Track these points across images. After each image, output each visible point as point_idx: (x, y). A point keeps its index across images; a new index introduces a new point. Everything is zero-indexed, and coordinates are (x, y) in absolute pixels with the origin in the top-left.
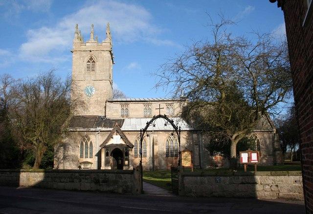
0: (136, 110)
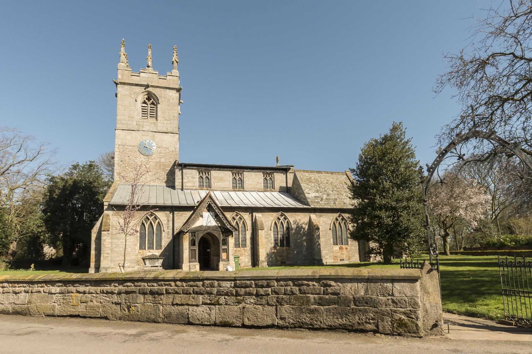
0: (221, 179)
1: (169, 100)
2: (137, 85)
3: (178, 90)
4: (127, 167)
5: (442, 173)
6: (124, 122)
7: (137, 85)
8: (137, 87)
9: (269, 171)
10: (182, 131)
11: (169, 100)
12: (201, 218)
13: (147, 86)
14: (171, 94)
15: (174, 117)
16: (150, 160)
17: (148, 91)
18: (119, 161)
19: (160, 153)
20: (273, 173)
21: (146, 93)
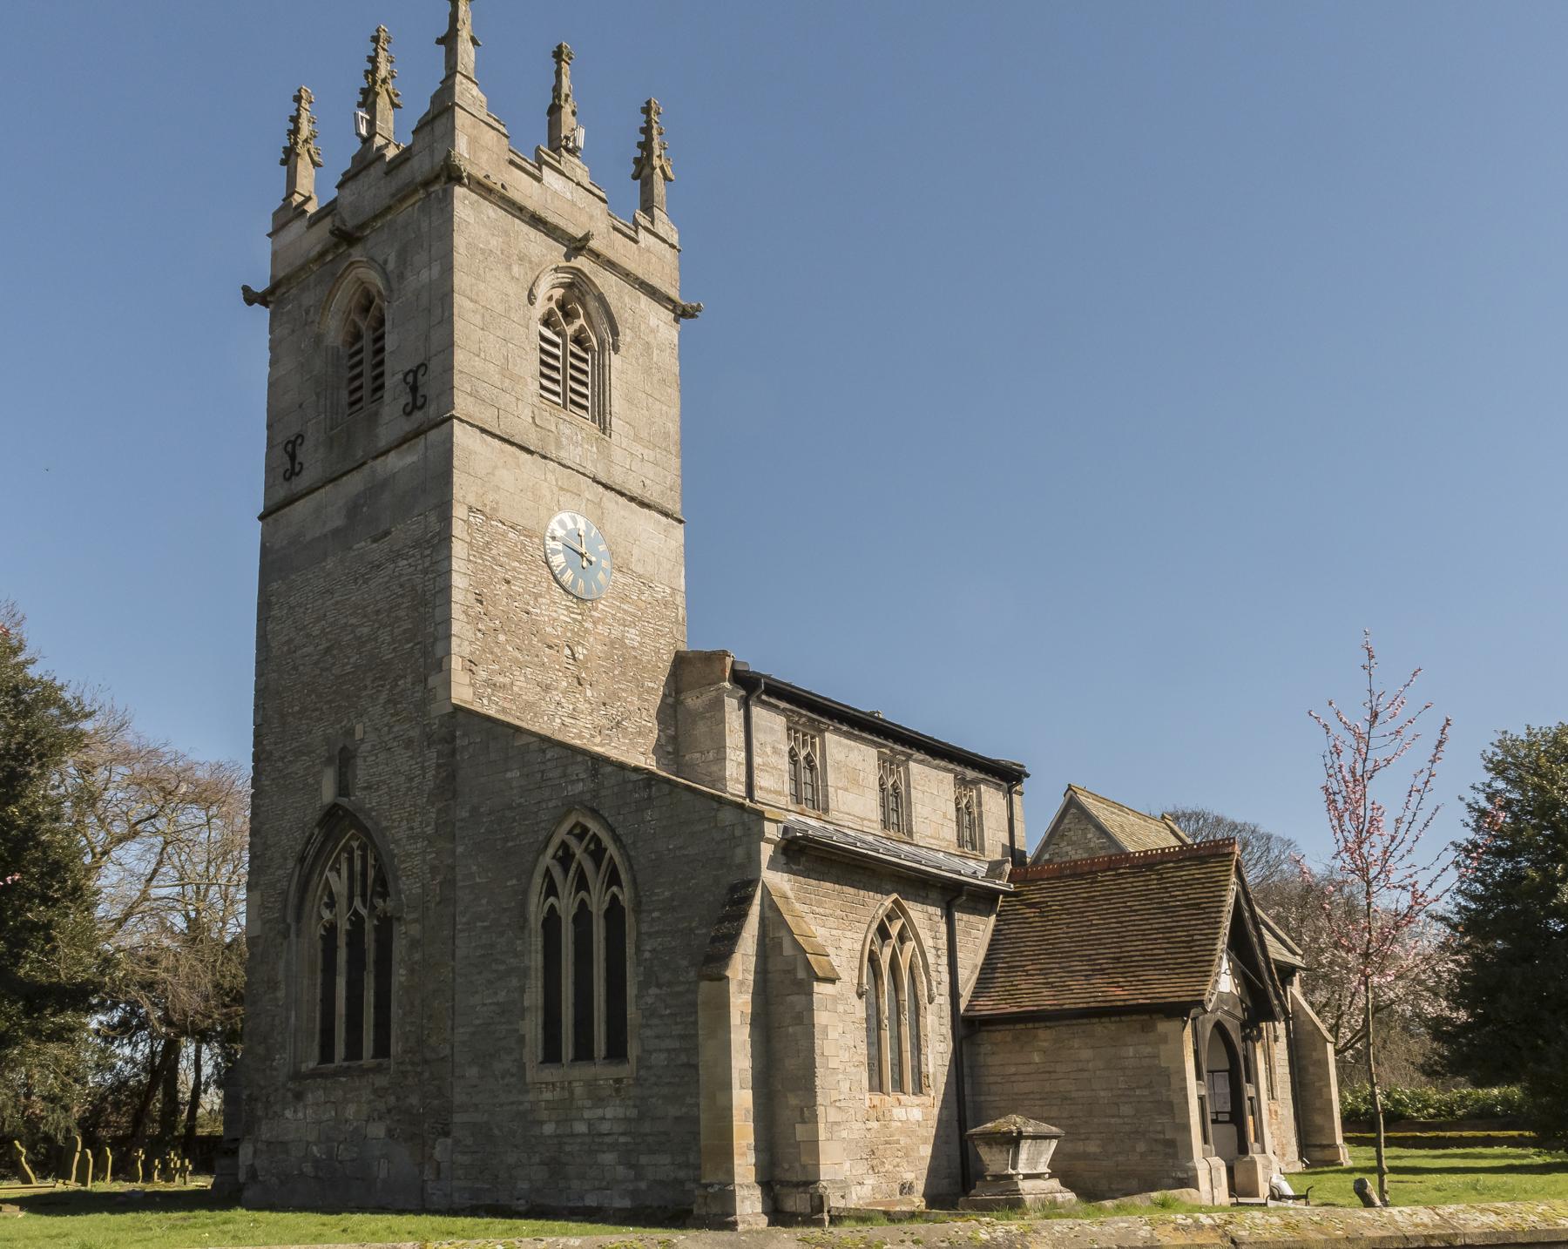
1: (648, 340)
2: (536, 221)
3: (682, 313)
4: (502, 638)
5: (136, 939)
6: (485, 391)
7: (536, 221)
8: (533, 234)
9: (970, 774)
10: (710, 503)
11: (648, 340)
12: (819, 988)
13: (578, 246)
14: (653, 321)
15: (667, 435)
16: (588, 625)
17: (577, 272)
18: (471, 597)
19: (624, 599)
20: (975, 782)
21: (566, 278)
